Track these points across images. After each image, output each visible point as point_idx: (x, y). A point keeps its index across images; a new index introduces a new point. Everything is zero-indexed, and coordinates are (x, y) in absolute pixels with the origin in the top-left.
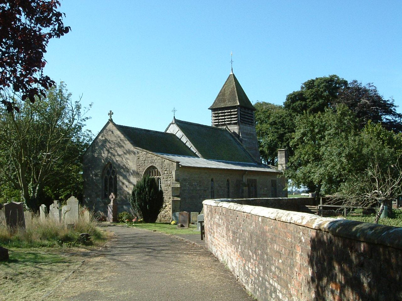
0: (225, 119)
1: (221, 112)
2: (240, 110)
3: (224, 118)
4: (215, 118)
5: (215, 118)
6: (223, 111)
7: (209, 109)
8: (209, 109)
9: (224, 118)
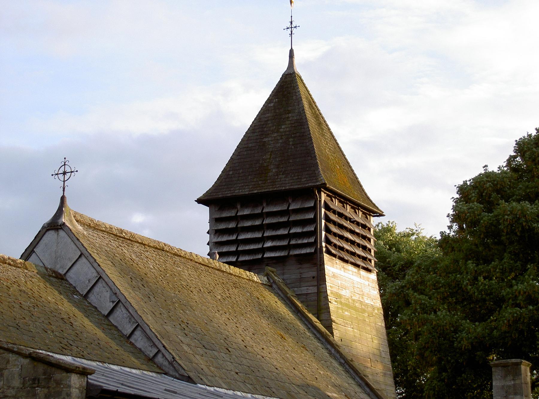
0: (263, 240)
1: (247, 212)
2: (327, 207)
3: (258, 235)
4: (225, 238)
5: (225, 238)
6: (258, 211)
7: (199, 201)
8: (199, 201)
9: (258, 235)
